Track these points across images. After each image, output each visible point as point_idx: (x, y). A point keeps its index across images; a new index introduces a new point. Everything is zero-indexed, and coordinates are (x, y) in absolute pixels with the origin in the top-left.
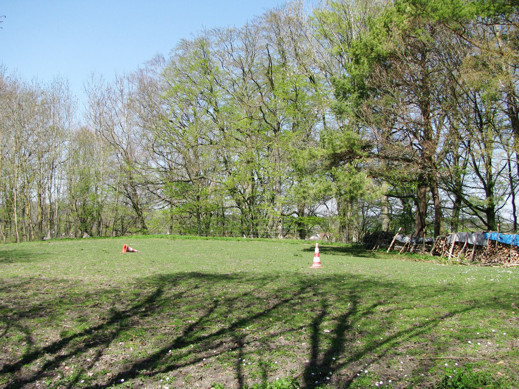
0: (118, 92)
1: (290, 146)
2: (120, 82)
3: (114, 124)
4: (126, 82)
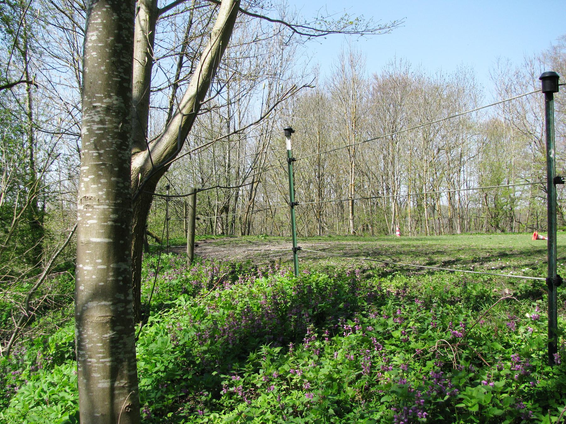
0: (528, 76)
1: (43, 101)
2: (530, 64)
3: (526, 112)
4: (537, 63)
